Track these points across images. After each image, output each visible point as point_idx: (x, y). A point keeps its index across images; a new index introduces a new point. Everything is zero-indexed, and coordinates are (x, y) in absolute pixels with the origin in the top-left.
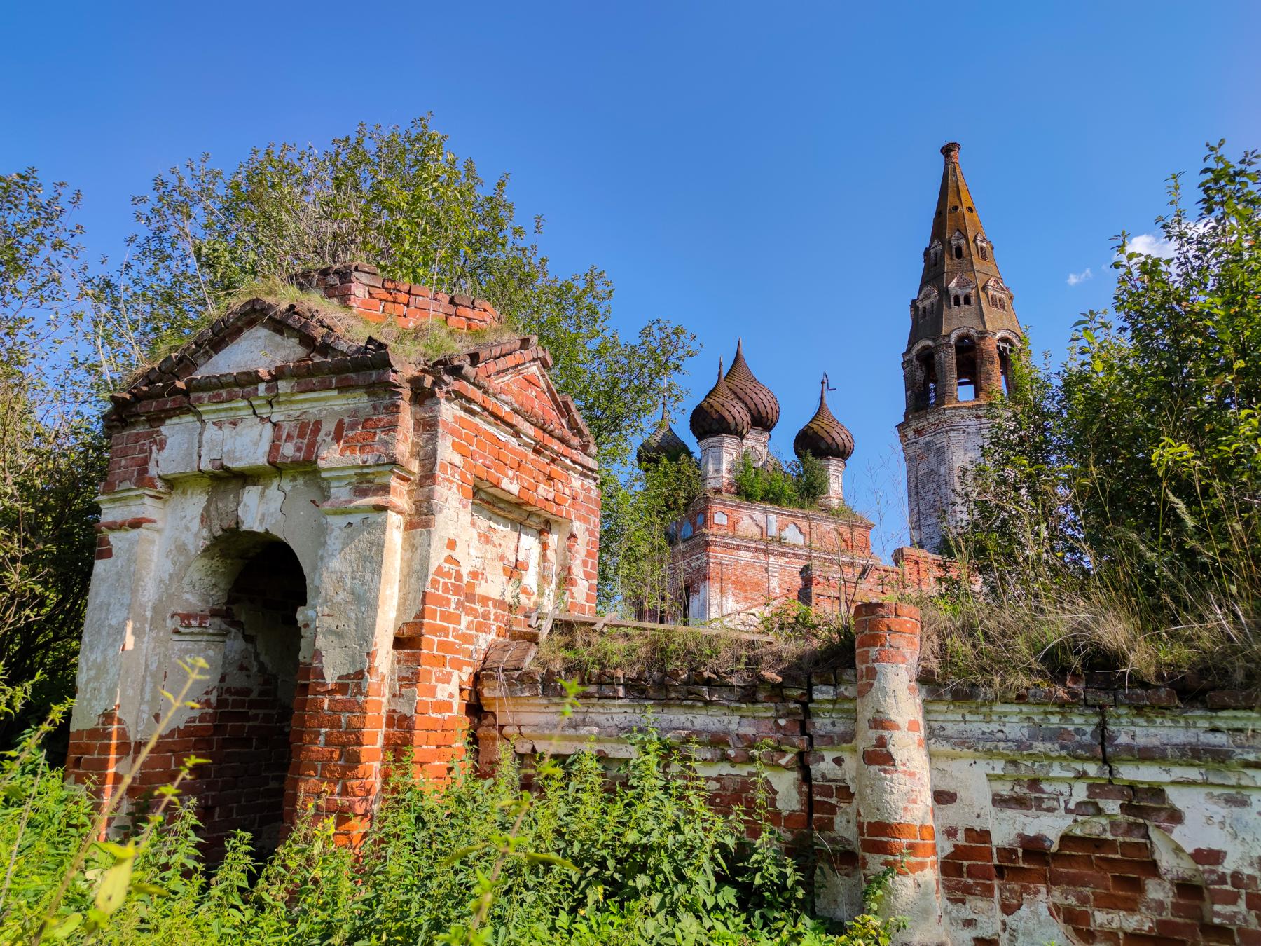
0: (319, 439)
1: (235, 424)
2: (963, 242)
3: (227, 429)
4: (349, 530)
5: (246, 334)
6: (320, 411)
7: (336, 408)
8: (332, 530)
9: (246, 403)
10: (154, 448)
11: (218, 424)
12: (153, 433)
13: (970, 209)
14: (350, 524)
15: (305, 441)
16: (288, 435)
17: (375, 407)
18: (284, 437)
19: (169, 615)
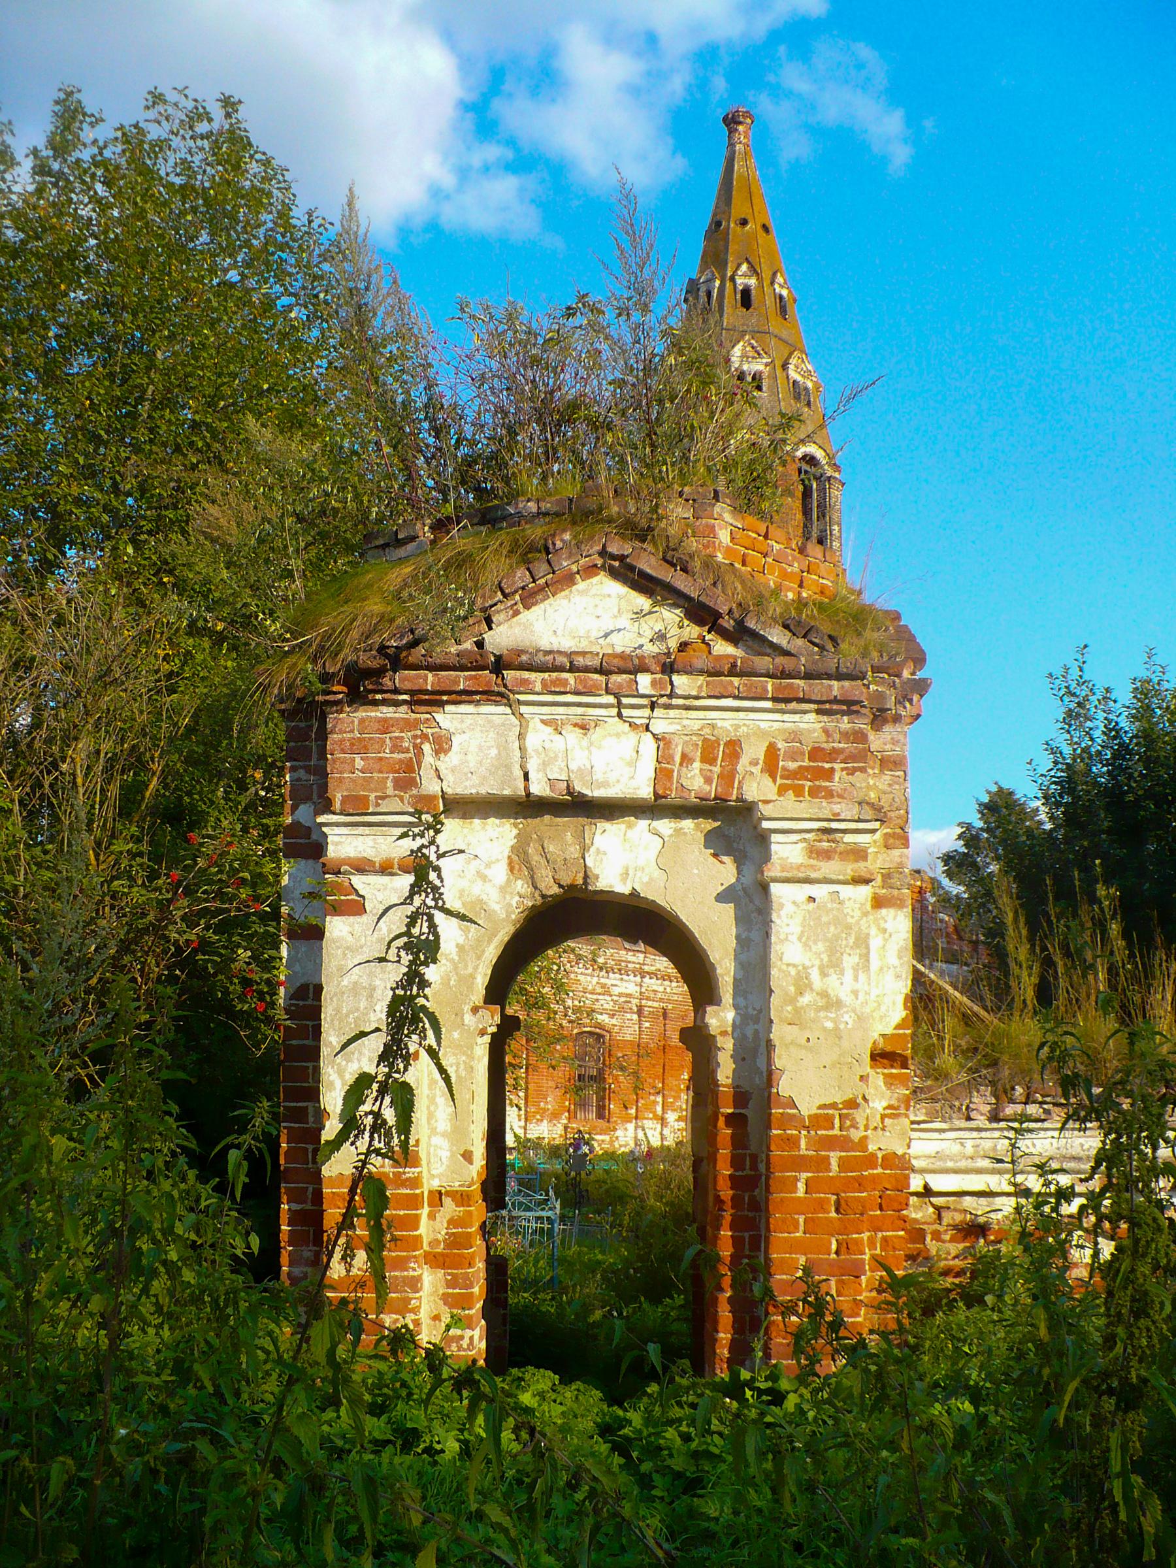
0: (739, 768)
1: (583, 727)
2: (753, 282)
3: (572, 736)
4: (812, 906)
5: (581, 585)
6: (737, 727)
7: (763, 725)
8: (782, 906)
9: (611, 699)
10: (426, 748)
11: (554, 725)
12: (417, 722)
13: (766, 228)
14: (812, 899)
15: (717, 769)
16: (684, 756)
17: (826, 731)
18: (678, 759)
19: (467, 1008)
